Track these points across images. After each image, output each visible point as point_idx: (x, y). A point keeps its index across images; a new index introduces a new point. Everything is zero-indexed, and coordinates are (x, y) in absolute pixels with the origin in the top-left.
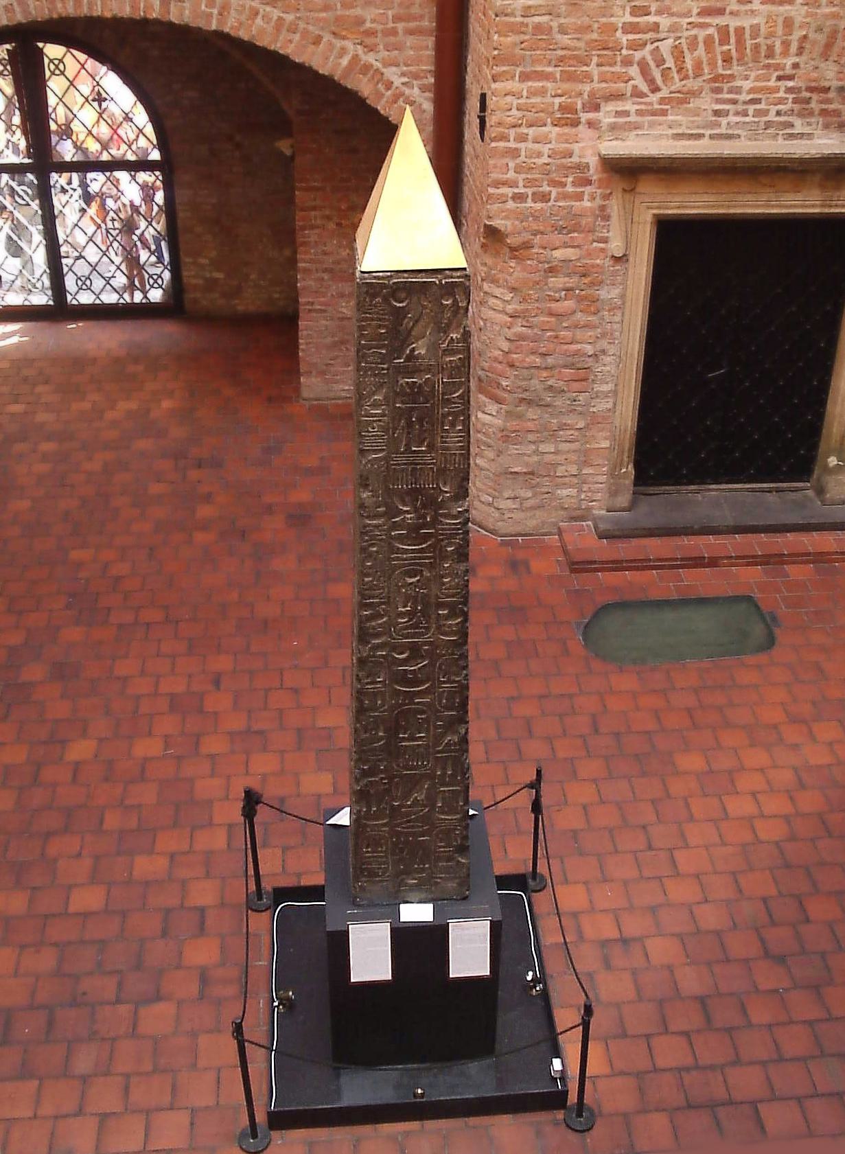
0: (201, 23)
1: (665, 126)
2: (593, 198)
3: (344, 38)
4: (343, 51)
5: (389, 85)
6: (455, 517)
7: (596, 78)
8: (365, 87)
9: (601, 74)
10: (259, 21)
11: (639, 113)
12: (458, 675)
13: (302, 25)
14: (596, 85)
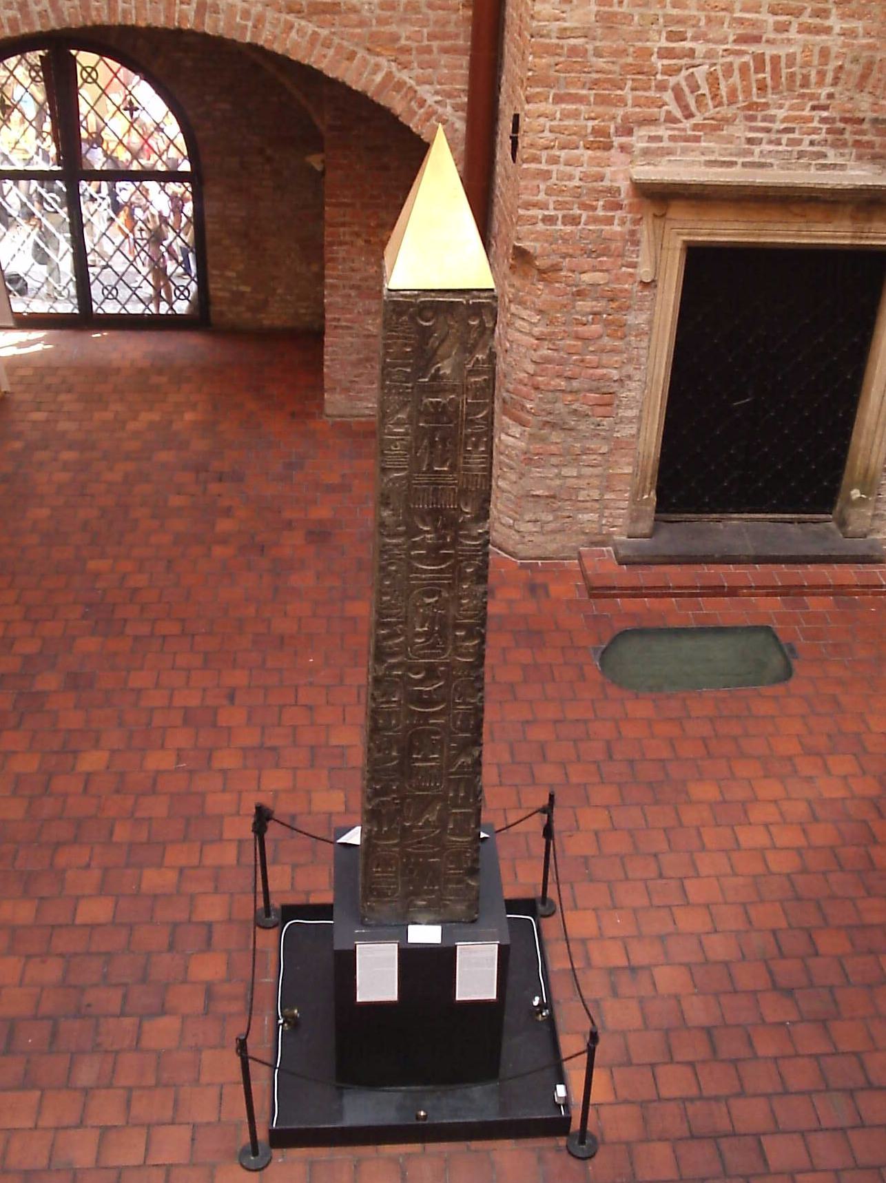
0: (235, 36)
1: (697, 153)
2: (623, 223)
3: (378, 54)
4: (377, 67)
5: (422, 103)
6: (475, 539)
7: (630, 102)
8: (397, 104)
9: (635, 98)
10: (293, 34)
11: (672, 138)
12: (473, 697)
13: (336, 40)
14: (629, 109)
